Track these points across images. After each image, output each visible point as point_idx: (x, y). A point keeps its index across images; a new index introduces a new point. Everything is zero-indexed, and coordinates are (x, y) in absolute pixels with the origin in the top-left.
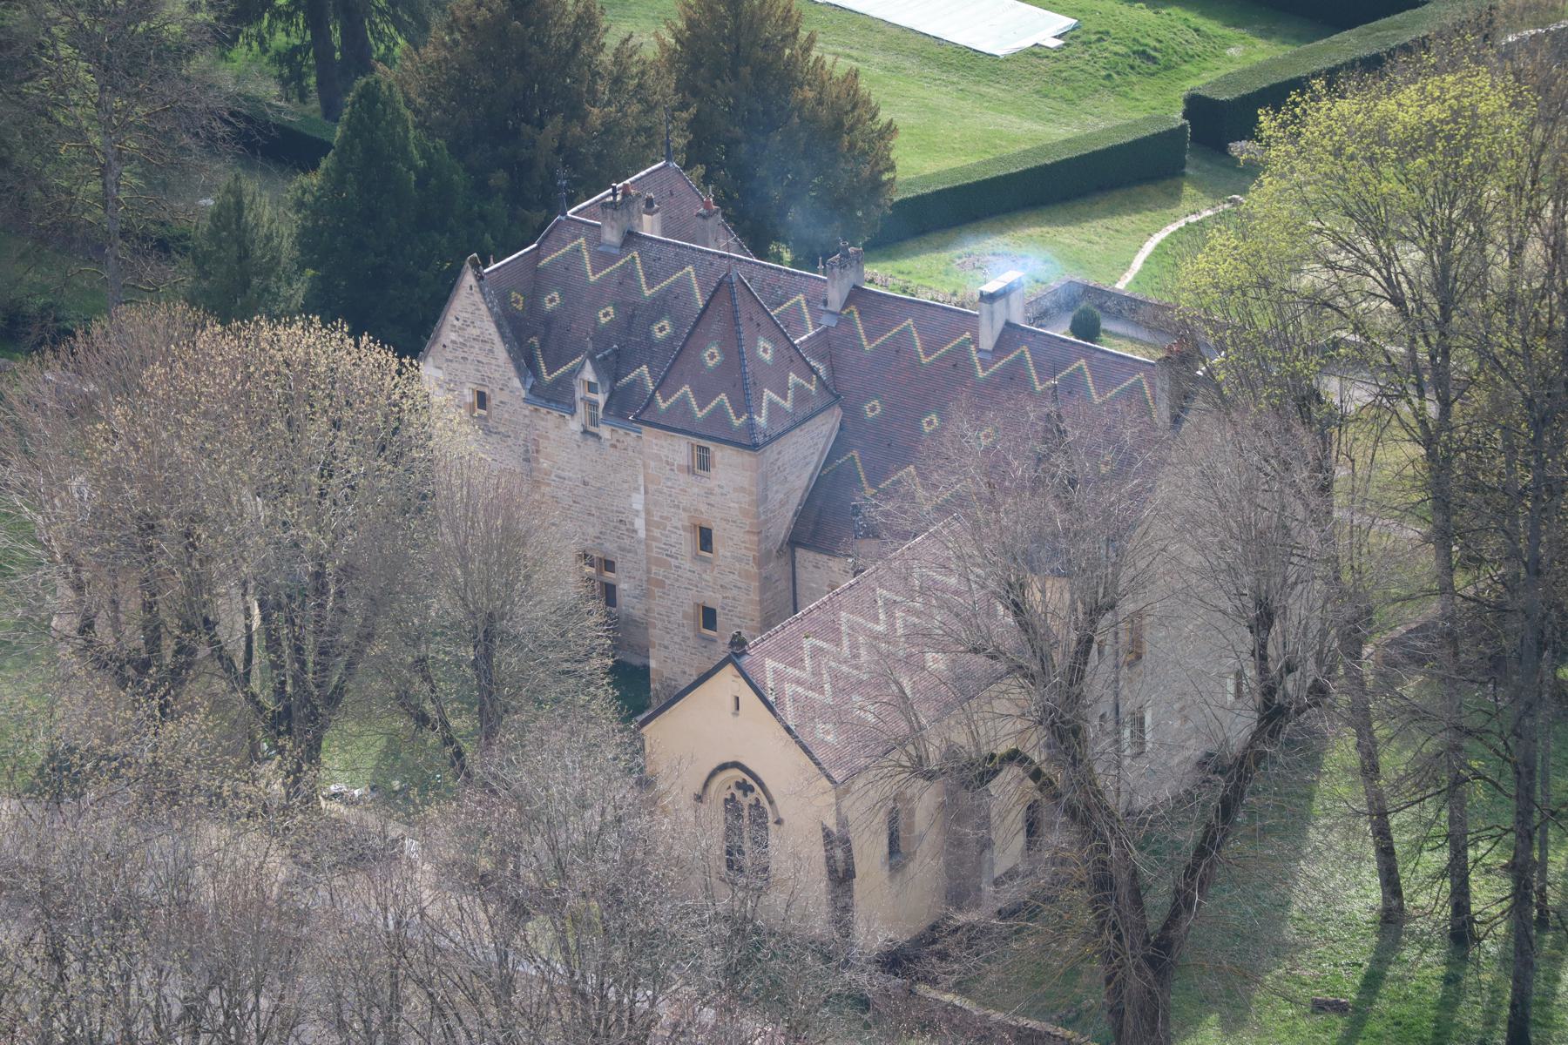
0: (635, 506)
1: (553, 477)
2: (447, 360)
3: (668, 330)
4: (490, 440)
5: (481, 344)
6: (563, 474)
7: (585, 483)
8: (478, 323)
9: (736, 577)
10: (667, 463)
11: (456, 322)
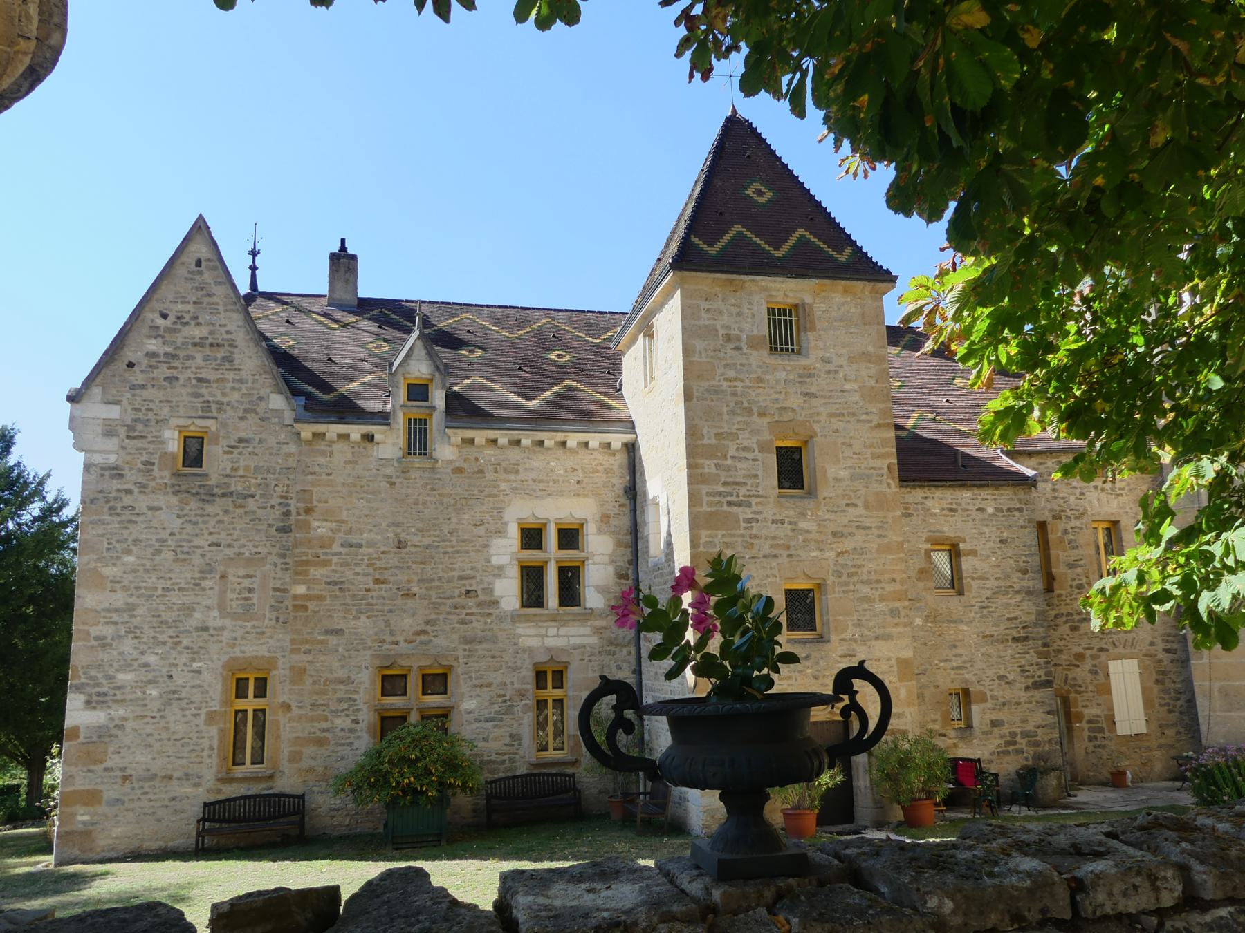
0: (495, 561)
1: (336, 548)
2: (133, 387)
3: (762, 200)
4: (210, 509)
5: (207, 351)
6: (354, 539)
7: (400, 545)
8: (205, 317)
9: (861, 511)
10: (728, 338)
11: (160, 322)
